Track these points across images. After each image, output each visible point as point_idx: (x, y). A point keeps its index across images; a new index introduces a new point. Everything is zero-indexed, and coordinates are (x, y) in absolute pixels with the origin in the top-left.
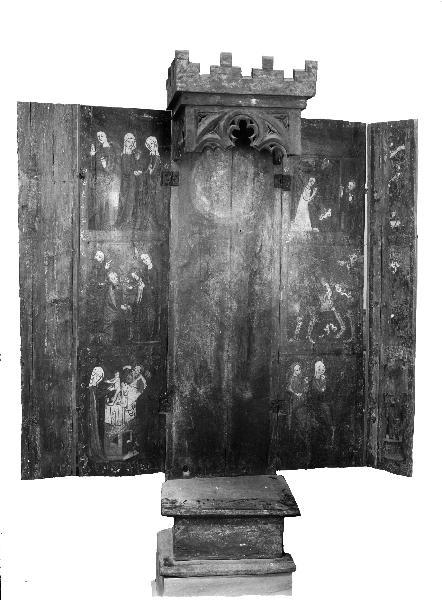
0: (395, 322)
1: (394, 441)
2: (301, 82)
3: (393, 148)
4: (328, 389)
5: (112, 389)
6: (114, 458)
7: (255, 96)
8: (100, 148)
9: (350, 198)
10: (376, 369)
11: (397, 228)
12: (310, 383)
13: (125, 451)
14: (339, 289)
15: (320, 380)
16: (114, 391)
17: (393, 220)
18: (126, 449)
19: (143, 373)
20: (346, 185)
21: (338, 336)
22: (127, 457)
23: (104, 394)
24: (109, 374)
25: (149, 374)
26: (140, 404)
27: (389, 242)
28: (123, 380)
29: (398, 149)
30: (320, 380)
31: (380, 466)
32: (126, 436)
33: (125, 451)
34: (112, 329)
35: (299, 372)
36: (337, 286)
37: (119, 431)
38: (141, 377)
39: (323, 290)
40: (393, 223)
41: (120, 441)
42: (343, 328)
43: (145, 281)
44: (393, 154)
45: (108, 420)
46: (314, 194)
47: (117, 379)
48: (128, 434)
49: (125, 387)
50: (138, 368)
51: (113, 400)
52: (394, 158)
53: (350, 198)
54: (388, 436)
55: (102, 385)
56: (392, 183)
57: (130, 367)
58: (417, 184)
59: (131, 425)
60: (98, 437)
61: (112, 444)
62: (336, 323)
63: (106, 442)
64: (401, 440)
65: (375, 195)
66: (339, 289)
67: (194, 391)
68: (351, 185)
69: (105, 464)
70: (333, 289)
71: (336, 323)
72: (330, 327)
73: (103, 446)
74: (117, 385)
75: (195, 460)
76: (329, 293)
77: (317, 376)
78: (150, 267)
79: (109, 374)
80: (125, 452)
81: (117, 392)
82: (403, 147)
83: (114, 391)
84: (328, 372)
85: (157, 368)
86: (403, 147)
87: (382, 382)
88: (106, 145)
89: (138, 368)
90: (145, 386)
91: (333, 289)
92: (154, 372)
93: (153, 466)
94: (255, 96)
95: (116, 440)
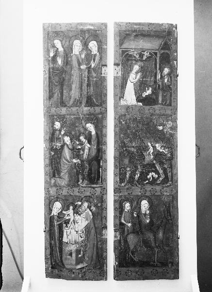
4: (151, 221)
5: (67, 218)
9: (166, 80)
12: (138, 216)
14: (158, 146)
16: (69, 220)
19: (89, 207)
21: (158, 182)
22: (79, 267)
24: (65, 207)
25: (93, 208)
26: (87, 229)
30: (145, 214)
31: (89, 280)
32: (78, 252)
34: (67, 176)
35: (128, 209)
36: (157, 145)
37: (73, 248)
38: (88, 210)
39: (146, 148)
41: (74, 255)
42: (163, 176)
43: (89, 142)
45: (65, 240)
47: (71, 211)
49: (77, 217)
51: (69, 225)
53: (166, 80)
55: (60, 215)
57: (80, 203)
61: (69, 257)
62: (157, 172)
68: (166, 71)
70: (154, 147)
71: (157, 172)
72: (152, 176)
73: (61, 257)
76: (151, 150)
77: (143, 212)
79: (65, 207)
80: (77, 263)
81: (71, 220)
83: (69, 220)
84: (150, 208)
88: (61, 49)
89: (86, 204)
91: (154, 147)
95: (71, 254)
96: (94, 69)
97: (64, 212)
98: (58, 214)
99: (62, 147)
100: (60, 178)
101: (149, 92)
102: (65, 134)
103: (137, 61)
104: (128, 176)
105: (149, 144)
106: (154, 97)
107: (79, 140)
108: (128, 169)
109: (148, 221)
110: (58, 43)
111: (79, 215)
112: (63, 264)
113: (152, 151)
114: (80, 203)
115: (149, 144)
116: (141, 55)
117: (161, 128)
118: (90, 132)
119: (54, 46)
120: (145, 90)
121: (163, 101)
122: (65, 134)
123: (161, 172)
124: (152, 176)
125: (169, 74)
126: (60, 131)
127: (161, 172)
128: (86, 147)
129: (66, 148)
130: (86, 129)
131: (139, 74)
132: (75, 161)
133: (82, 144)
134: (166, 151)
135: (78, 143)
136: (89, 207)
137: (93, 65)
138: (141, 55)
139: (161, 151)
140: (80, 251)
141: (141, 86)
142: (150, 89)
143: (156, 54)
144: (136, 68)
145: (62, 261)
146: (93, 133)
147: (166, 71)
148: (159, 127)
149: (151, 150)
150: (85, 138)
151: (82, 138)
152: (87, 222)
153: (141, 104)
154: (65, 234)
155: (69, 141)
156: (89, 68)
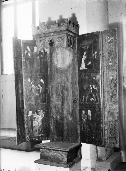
0: (112, 97)
1: (113, 136)
2: (63, 26)
3: (109, 39)
6: (36, 136)
7: (52, 32)
8: (28, 51)
9: (96, 57)
10: (106, 113)
11: (111, 65)
12: (87, 116)
13: (39, 134)
14: (94, 86)
15: (90, 116)
16: (35, 118)
17: (110, 62)
18: (39, 133)
19: (43, 112)
20: (94, 53)
21: (94, 102)
22: (40, 135)
23: (32, 118)
24: (34, 113)
25: (44, 112)
27: (109, 70)
28: (38, 114)
29: (111, 39)
30: (90, 116)
32: (39, 130)
33: (39, 134)
37: (38, 128)
39: (89, 87)
40: (110, 64)
41: (38, 131)
42: (96, 100)
43: (42, 87)
44: (109, 40)
45: (34, 125)
46: (86, 57)
47: (36, 114)
48: (40, 129)
49: (38, 116)
50: (41, 111)
51: (35, 120)
52: (109, 42)
54: (110, 135)
55: (32, 116)
56: (109, 50)
57: (39, 111)
58: (122, 33)
59: (40, 126)
60: (31, 130)
62: (94, 98)
63: (34, 131)
64: (115, 136)
65: (104, 55)
66: (94, 86)
67: (56, 117)
68: (96, 53)
69: (34, 138)
70: (92, 87)
72: (92, 99)
73: (33, 132)
74: (36, 115)
75: (58, 137)
76: (91, 88)
77: (89, 115)
78: (43, 83)
80: (39, 134)
81: (36, 118)
82: (112, 38)
83: (35, 118)
84: (92, 113)
85: (47, 111)
86: (112, 38)
87: (108, 117)
88: (29, 50)
89: (41, 111)
90: (44, 116)
91: (92, 87)
92: (46, 112)
93: (47, 137)
94: (52, 32)
95: (36, 131)
96: (43, 58)
97: (33, 115)
98: (31, 115)
99: (32, 89)
100: (31, 101)
101: (90, 63)
102: (33, 84)
103: (85, 50)
104: (83, 99)
105: (90, 86)
106: (92, 65)
107: (38, 86)
108: (83, 96)
109: (91, 119)
110: (28, 48)
111: (39, 115)
112: (34, 135)
113: (91, 89)
114: (39, 111)
115: (90, 86)
116: (86, 48)
117: (94, 78)
118: (42, 83)
119: (26, 49)
120: (88, 63)
121: (95, 67)
122: (33, 84)
123: (95, 98)
124: (92, 99)
125: (97, 54)
126: (30, 83)
127: (95, 98)
128: (41, 89)
129: (33, 89)
130: (40, 82)
131: (86, 56)
132: (36, 94)
133: (39, 87)
134: (96, 89)
135: (37, 87)
136: (43, 112)
137: (42, 57)
138: (86, 48)
139: (95, 88)
140: (40, 129)
141: (86, 62)
142: (90, 62)
143: (92, 46)
144: (85, 53)
145: (33, 134)
146: (43, 83)
147: (96, 53)
148: (94, 78)
149: (91, 88)
150: (40, 85)
151: (39, 85)
152: (42, 118)
153: (87, 69)
154: (34, 123)
155: (34, 87)
156: (41, 58)
